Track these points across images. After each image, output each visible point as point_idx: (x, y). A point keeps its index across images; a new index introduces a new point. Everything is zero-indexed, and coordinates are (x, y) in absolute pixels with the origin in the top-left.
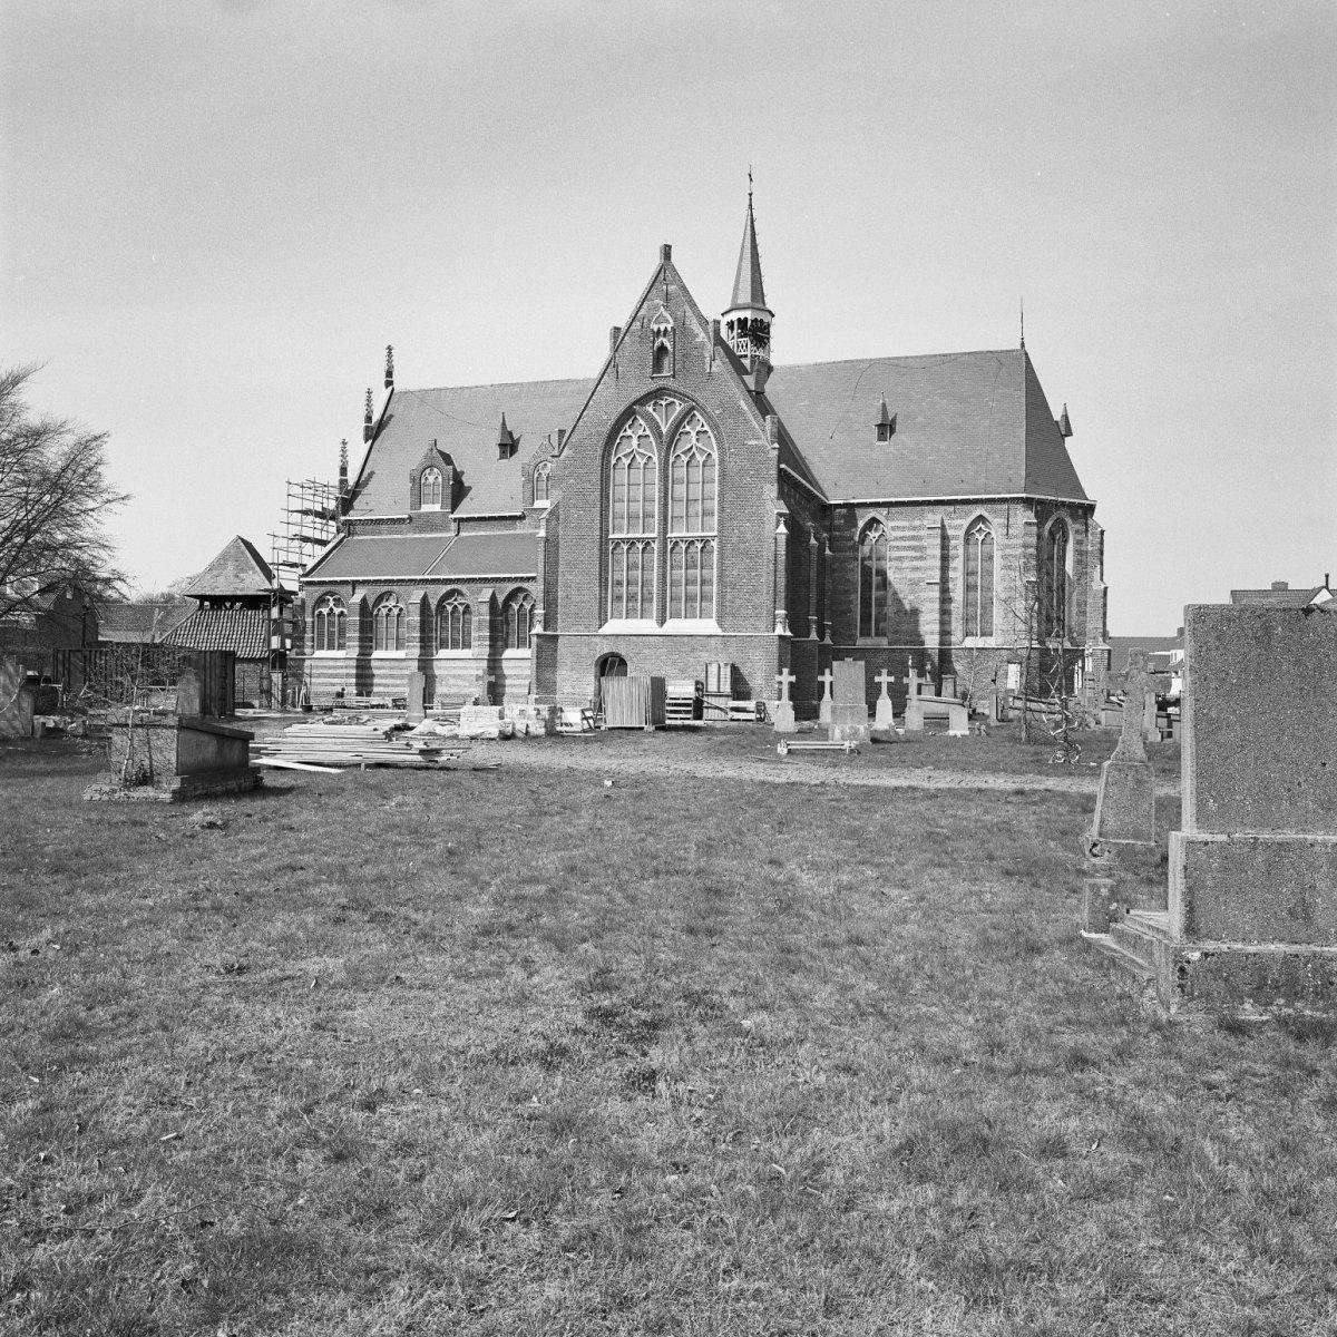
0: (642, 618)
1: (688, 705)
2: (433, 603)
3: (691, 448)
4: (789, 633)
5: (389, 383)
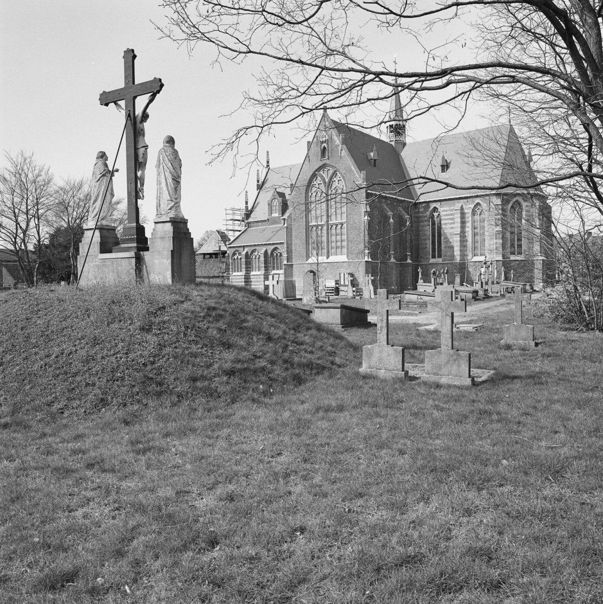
1: (332, 290)
2: (269, 252)
4: (370, 260)
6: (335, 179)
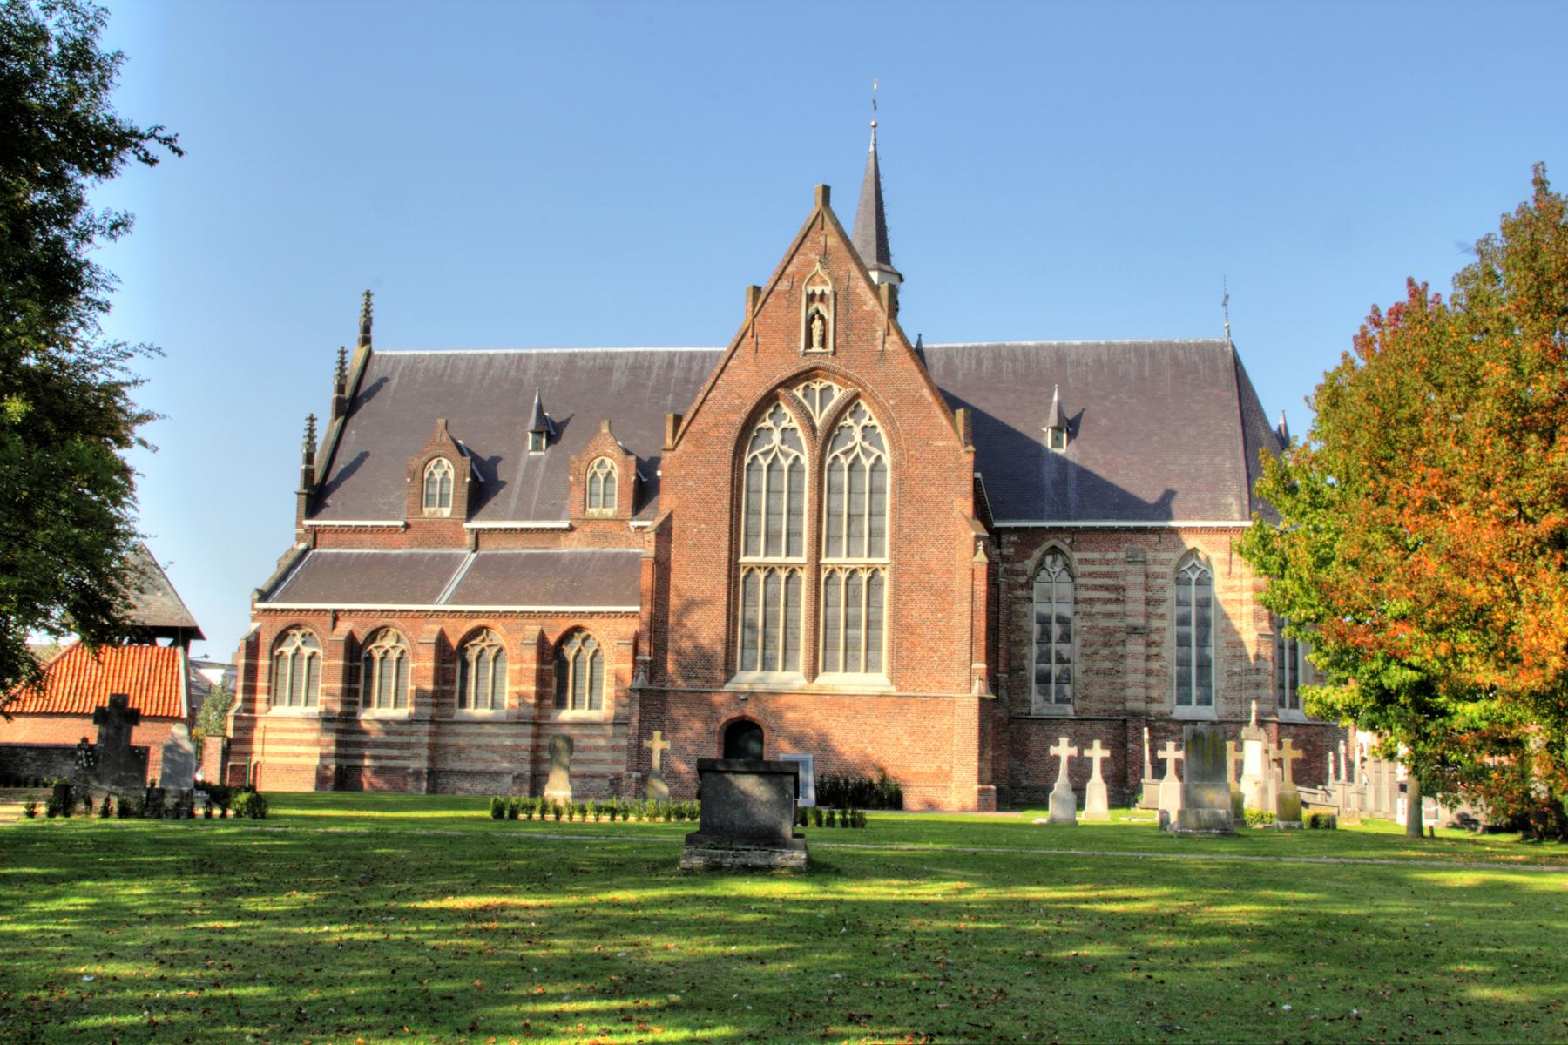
0: (845, 670)
3: (853, 448)
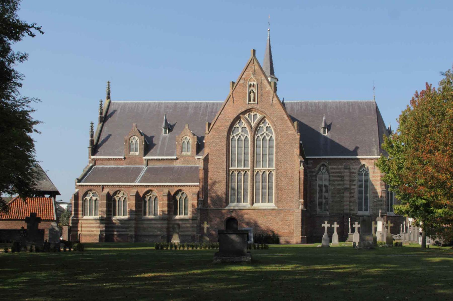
3: (264, 134)
5: (109, 98)
6: (238, 126)
